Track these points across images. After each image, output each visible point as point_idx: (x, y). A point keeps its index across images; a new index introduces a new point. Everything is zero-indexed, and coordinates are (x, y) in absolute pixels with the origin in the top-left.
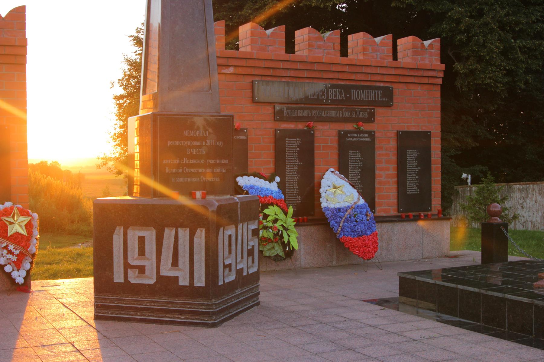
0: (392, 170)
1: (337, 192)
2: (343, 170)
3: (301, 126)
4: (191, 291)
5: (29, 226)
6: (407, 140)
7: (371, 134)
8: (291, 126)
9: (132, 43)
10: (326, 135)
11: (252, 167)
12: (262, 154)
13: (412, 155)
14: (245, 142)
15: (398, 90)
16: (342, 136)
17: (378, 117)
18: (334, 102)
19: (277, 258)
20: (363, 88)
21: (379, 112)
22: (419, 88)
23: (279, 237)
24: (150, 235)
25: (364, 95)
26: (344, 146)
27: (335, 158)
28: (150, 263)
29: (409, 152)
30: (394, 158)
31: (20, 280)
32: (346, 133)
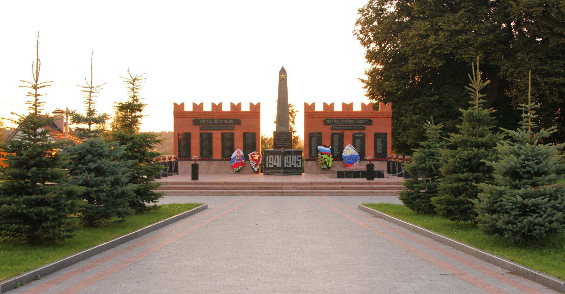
0: (372, 145)
1: (349, 151)
2: (354, 145)
3: (340, 132)
4: (279, 168)
5: (259, 158)
6: (377, 135)
7: (364, 134)
8: (336, 132)
9: (368, 98)
10: (348, 135)
11: (323, 144)
12: (326, 139)
13: (379, 140)
14: (321, 137)
15: (374, 120)
16: (354, 135)
17: (235, 128)
18: (350, 124)
19: (325, 169)
20: (361, 120)
21: (367, 127)
22: (383, 119)
23: (325, 162)
24: (272, 157)
25: (361, 122)
26: (354, 138)
27: (351, 141)
28: (272, 163)
29: (378, 139)
30: (373, 141)
31: (256, 170)
32: (355, 134)
